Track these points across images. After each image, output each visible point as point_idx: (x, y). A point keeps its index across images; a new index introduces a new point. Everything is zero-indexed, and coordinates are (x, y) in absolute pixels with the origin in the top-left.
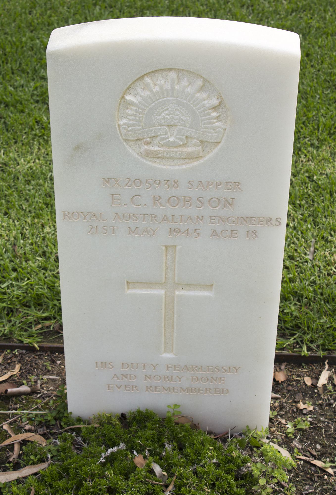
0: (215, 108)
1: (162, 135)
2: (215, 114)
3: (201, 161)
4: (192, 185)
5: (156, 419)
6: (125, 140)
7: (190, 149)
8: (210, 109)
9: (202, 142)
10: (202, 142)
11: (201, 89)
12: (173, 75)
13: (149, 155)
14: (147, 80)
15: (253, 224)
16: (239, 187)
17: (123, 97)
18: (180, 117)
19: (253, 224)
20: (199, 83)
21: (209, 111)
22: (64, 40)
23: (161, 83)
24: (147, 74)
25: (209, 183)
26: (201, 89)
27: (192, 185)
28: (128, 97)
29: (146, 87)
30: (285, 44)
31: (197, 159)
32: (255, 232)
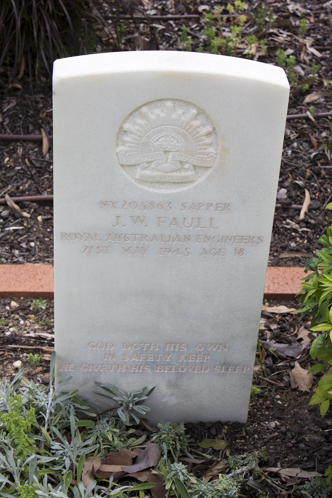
0: (208, 134)
1: (156, 160)
2: (208, 140)
3: (194, 184)
4: (185, 206)
5: (48, 339)
6: (122, 166)
7: (183, 174)
8: (205, 135)
9: (194, 166)
10: (194, 166)
11: (195, 117)
12: (169, 104)
13: (143, 180)
14: (145, 109)
15: (260, 239)
16: (228, 209)
17: (122, 127)
18: (175, 144)
19: (260, 239)
20: (194, 111)
21: (203, 137)
22: (65, 69)
23: (155, 113)
24: (144, 105)
25: (201, 205)
26: (195, 117)
27: (185, 206)
28: (127, 126)
29: (143, 116)
30: (275, 77)
31: (183, 184)
32: (242, 250)
